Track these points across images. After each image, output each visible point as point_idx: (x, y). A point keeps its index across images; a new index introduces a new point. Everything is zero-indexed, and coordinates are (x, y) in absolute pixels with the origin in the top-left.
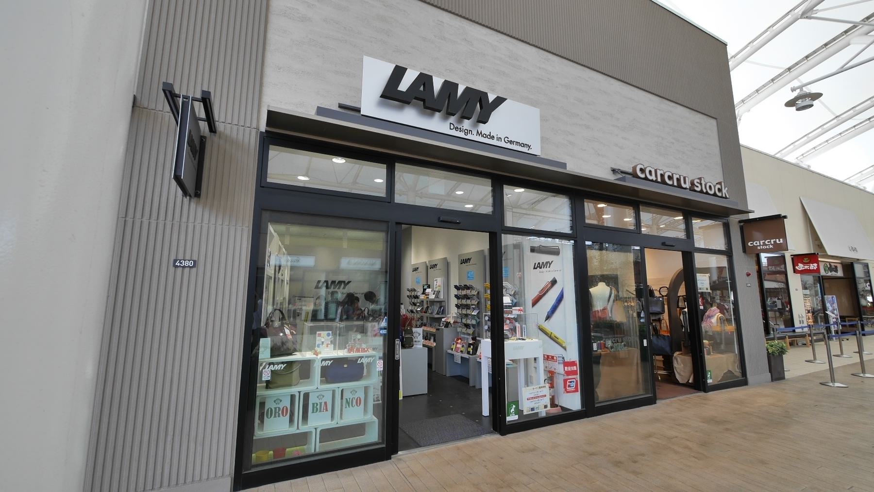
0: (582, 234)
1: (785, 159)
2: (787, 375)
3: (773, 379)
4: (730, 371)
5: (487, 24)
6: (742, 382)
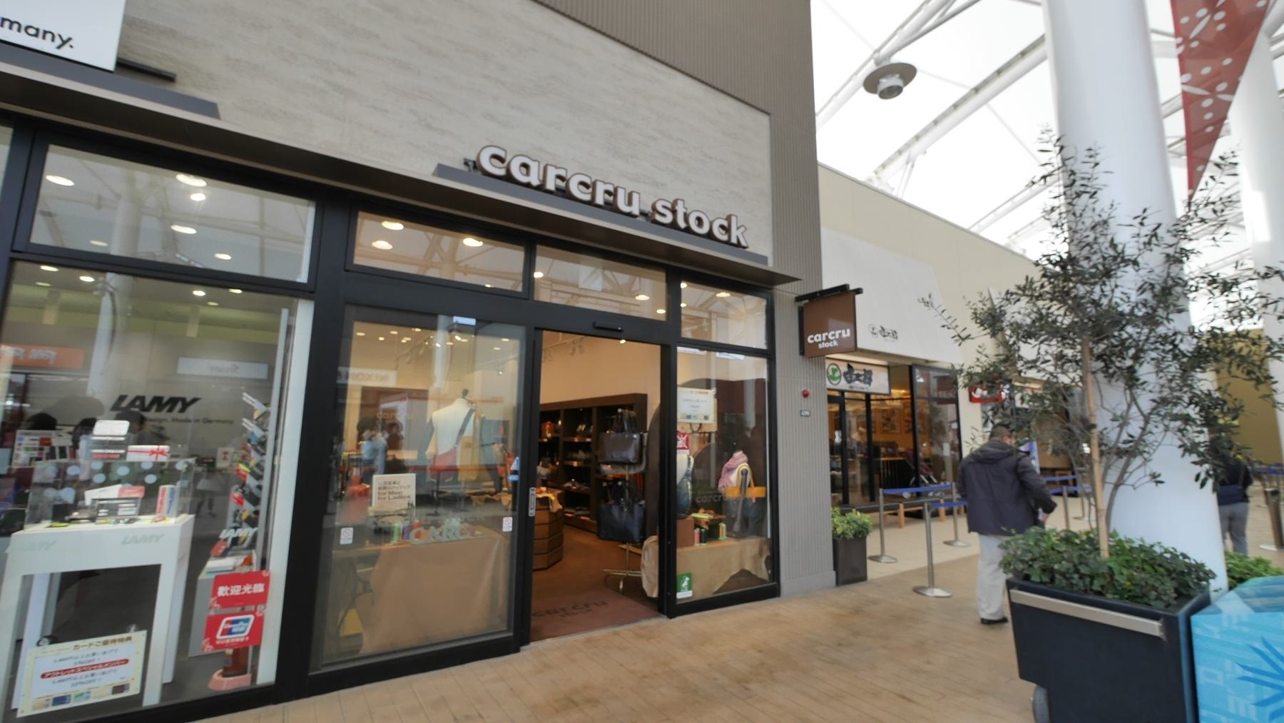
0: (347, 298)
1: (983, 234)
2: (873, 570)
3: (841, 581)
4: (743, 573)
5: (579, 18)
6: (770, 591)
